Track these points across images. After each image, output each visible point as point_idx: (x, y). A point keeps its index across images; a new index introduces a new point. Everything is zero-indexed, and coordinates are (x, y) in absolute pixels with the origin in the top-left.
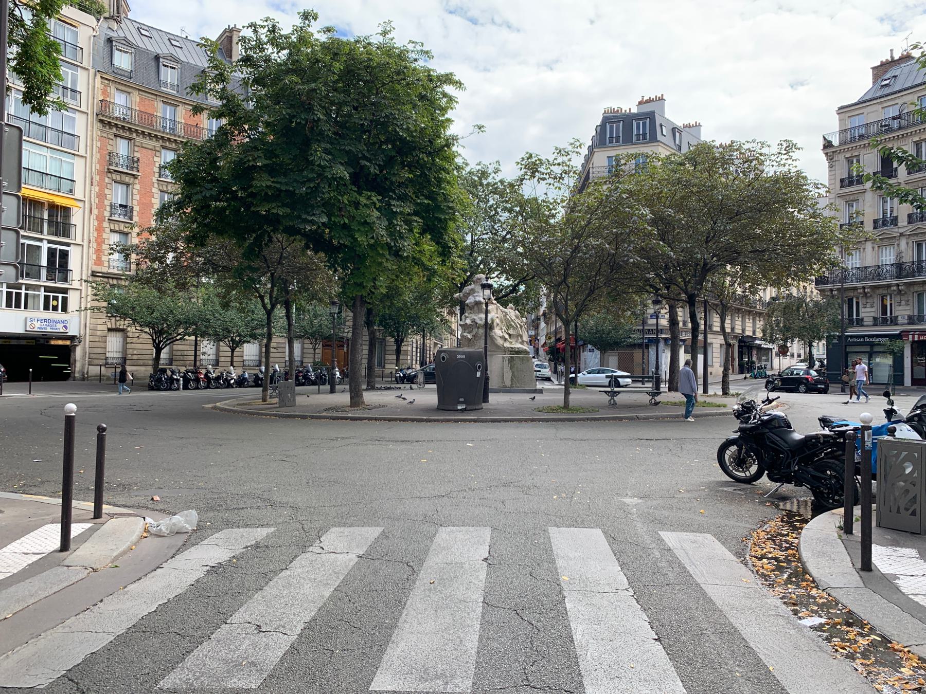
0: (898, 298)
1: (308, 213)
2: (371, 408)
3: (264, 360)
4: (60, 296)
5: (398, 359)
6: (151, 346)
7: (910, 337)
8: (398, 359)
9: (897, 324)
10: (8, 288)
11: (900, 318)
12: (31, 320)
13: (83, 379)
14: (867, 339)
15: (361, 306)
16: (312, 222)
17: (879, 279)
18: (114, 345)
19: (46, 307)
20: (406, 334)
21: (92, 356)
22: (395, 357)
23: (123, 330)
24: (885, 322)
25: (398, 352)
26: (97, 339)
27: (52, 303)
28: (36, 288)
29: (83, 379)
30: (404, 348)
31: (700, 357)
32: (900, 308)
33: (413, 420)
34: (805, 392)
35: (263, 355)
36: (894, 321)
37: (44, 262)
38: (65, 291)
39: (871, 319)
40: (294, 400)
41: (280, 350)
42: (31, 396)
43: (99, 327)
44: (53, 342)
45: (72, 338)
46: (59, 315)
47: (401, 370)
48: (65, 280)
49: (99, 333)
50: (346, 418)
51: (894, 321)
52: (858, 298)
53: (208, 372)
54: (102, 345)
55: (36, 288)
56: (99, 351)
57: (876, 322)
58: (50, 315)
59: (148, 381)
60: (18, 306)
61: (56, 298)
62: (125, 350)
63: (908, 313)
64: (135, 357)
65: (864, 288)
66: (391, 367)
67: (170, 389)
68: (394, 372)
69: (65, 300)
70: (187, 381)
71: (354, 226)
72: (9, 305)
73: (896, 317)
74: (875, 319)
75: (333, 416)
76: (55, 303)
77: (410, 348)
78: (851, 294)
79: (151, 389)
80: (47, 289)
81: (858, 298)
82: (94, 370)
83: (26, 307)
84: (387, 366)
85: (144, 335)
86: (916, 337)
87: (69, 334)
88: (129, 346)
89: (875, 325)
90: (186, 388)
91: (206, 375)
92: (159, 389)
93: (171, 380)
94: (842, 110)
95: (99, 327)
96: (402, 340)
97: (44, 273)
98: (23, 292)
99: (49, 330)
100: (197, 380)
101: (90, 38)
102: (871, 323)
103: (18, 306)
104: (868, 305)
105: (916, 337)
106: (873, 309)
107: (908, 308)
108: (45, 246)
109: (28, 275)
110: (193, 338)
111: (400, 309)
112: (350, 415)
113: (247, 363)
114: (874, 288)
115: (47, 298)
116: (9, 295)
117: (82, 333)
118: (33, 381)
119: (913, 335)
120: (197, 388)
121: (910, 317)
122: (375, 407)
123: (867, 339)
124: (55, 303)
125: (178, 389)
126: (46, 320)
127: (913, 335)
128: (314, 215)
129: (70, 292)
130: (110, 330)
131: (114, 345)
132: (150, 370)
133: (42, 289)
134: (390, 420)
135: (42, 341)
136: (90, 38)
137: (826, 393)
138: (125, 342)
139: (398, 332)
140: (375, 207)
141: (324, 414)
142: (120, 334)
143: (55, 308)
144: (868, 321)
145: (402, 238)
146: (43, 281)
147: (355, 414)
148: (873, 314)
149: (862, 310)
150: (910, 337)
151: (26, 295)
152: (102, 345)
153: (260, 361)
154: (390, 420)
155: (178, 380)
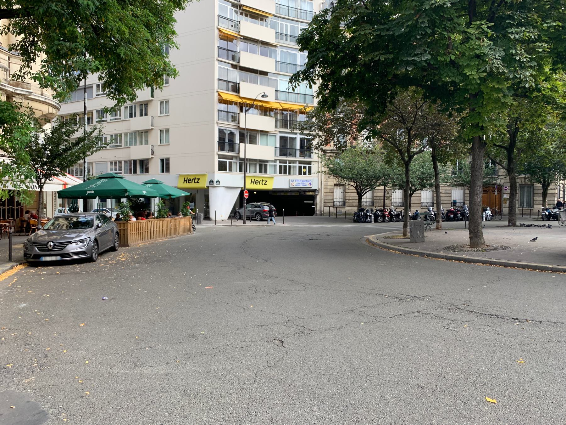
1: (410, 55)
2: (490, 249)
3: (435, 202)
4: (307, 166)
5: (544, 201)
6: (356, 195)
8: (544, 201)
10: (280, 163)
12: (292, 181)
13: (321, 215)
15: (480, 148)
16: (414, 63)
18: (338, 194)
19: (300, 173)
20: (553, 180)
21: (326, 201)
22: (541, 199)
23: (343, 185)
25: (545, 195)
26: (328, 191)
27: (303, 170)
28: (294, 162)
29: (321, 215)
30: (549, 192)
33: (535, 268)
35: (435, 198)
37: (298, 147)
38: (310, 163)
40: (423, 237)
41: (447, 195)
42: (284, 225)
43: (329, 184)
44: (308, 193)
45: (315, 191)
46: (306, 177)
47: (547, 210)
48: (310, 156)
49: (329, 187)
50: (459, 259)
53: (391, 211)
54: (331, 194)
55: (294, 162)
56: (330, 198)
58: (302, 177)
59: (352, 216)
60: (285, 173)
61: (305, 167)
62: (344, 197)
64: (351, 201)
66: (538, 207)
67: (365, 222)
68: (541, 210)
69: (310, 168)
70: (376, 217)
71: (463, 62)
72: (280, 173)
75: (451, 256)
76: (304, 170)
77: (557, 192)
79: (355, 221)
80: (300, 162)
82: (326, 209)
83: (289, 173)
84: (535, 206)
85: (351, 188)
87: (313, 188)
88: (347, 194)
90: (376, 221)
91: (390, 213)
92: (358, 222)
93: (366, 216)
95: (329, 184)
96: (548, 185)
97: (298, 153)
98: (288, 165)
99: (301, 186)
100: (384, 216)
101: (320, 5)
103: (285, 173)
108: (298, 137)
109: (290, 155)
110: (382, 188)
111: (544, 157)
112: (465, 256)
113: (423, 204)
115: (300, 167)
116: (281, 167)
117: (320, 187)
118: (286, 215)
120: (383, 221)
122: (495, 249)
124: (304, 170)
125: (371, 222)
126: (300, 181)
128: (416, 55)
129: (313, 163)
130: (335, 185)
131: (338, 194)
132: (355, 209)
133: (298, 162)
134: (507, 265)
135: (302, 193)
136: (320, 5)
138: (344, 192)
139: (544, 178)
140: (486, 37)
141: (441, 253)
142: (342, 187)
143: (305, 173)
145: (522, 68)
146: (298, 158)
147: (474, 257)
151: (290, 167)
152: (331, 194)
153: (433, 203)
154: (507, 265)
155: (370, 216)
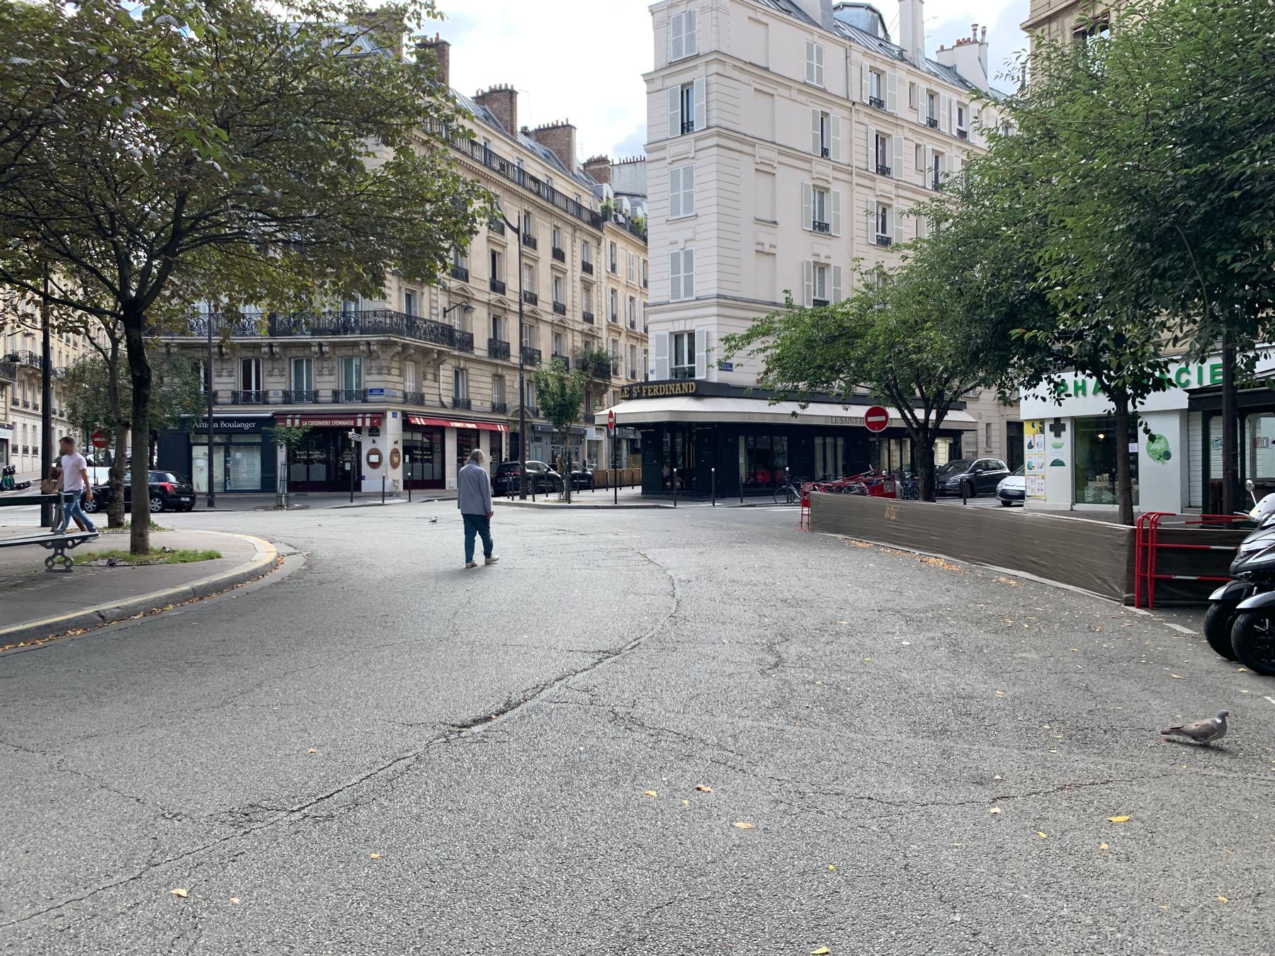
0: (368, 363)
7: (289, 422)
9: (266, 403)
11: (271, 394)
14: (223, 425)
17: (244, 334)
24: (247, 399)
31: (1217, 472)
32: (272, 380)
34: (162, 511)
36: (262, 398)
39: (230, 394)
51: (262, 398)
52: (309, 361)
57: (236, 399)
63: (284, 387)
65: (320, 345)
73: (266, 393)
74: (235, 394)
78: (199, 354)
81: (309, 361)
86: (297, 422)
89: (235, 403)
94: (1030, 28)
102: (229, 400)
104: (225, 373)
105: (297, 422)
106: (232, 380)
107: (283, 380)
114: (285, 346)
119: (293, 420)
121: (286, 394)
123: (223, 425)
127: (293, 420)
137: (189, 510)
144: (325, 394)
148: (231, 387)
149: (215, 380)
150: (289, 422)
